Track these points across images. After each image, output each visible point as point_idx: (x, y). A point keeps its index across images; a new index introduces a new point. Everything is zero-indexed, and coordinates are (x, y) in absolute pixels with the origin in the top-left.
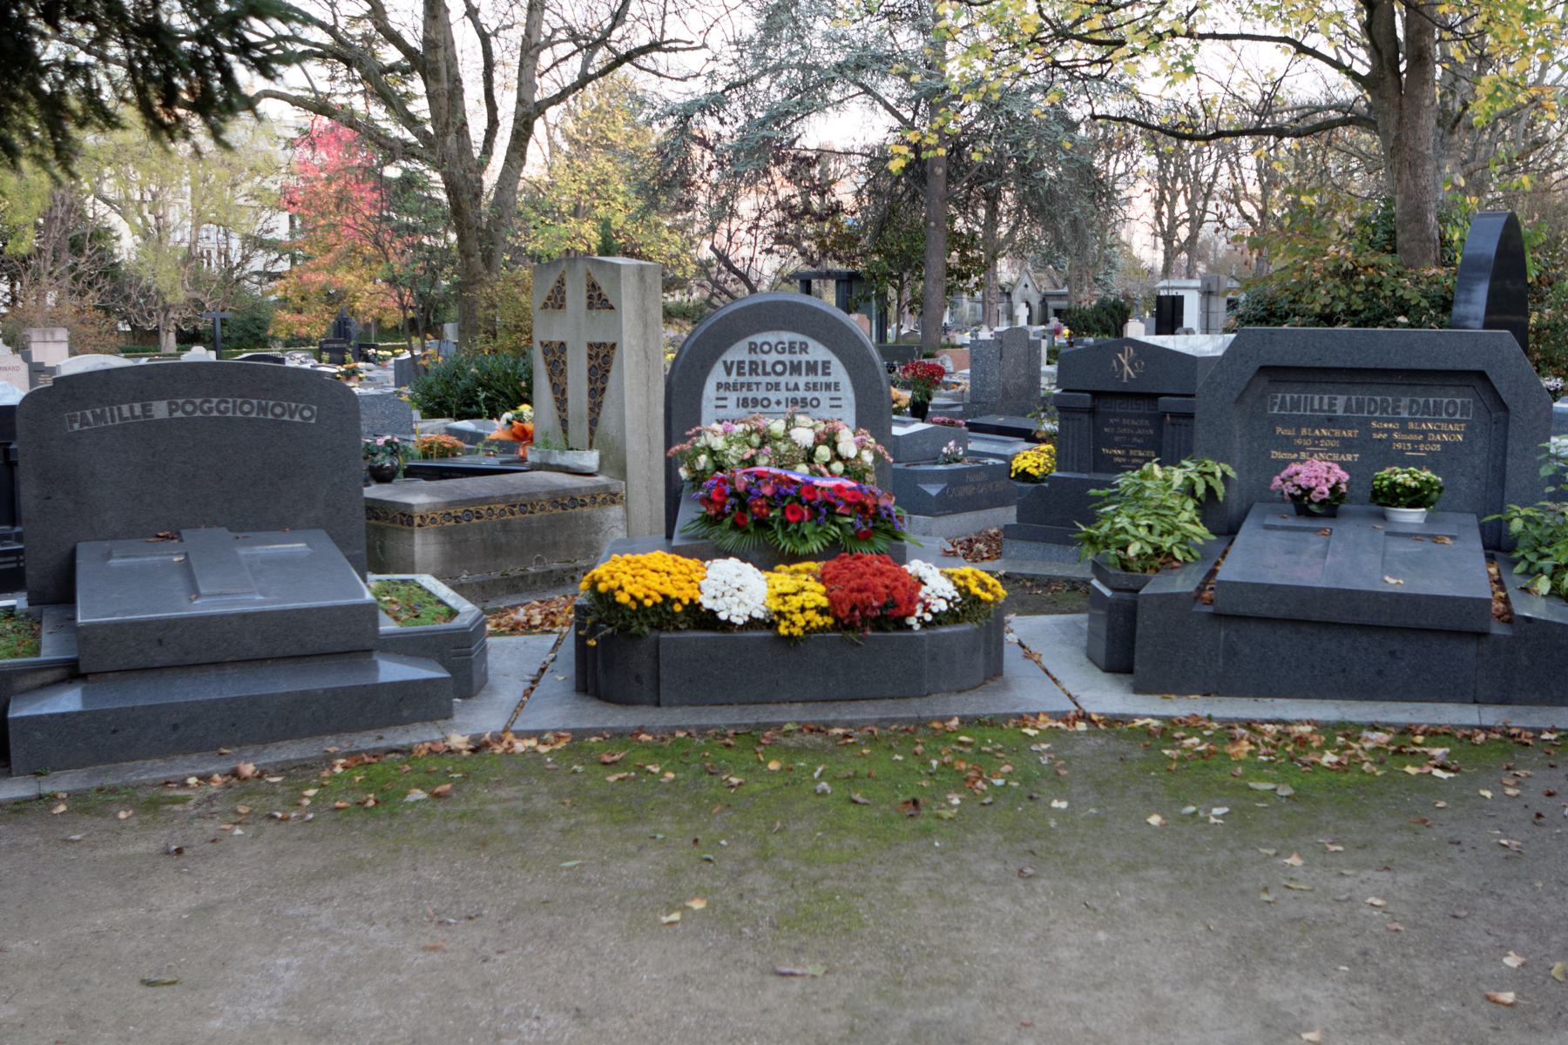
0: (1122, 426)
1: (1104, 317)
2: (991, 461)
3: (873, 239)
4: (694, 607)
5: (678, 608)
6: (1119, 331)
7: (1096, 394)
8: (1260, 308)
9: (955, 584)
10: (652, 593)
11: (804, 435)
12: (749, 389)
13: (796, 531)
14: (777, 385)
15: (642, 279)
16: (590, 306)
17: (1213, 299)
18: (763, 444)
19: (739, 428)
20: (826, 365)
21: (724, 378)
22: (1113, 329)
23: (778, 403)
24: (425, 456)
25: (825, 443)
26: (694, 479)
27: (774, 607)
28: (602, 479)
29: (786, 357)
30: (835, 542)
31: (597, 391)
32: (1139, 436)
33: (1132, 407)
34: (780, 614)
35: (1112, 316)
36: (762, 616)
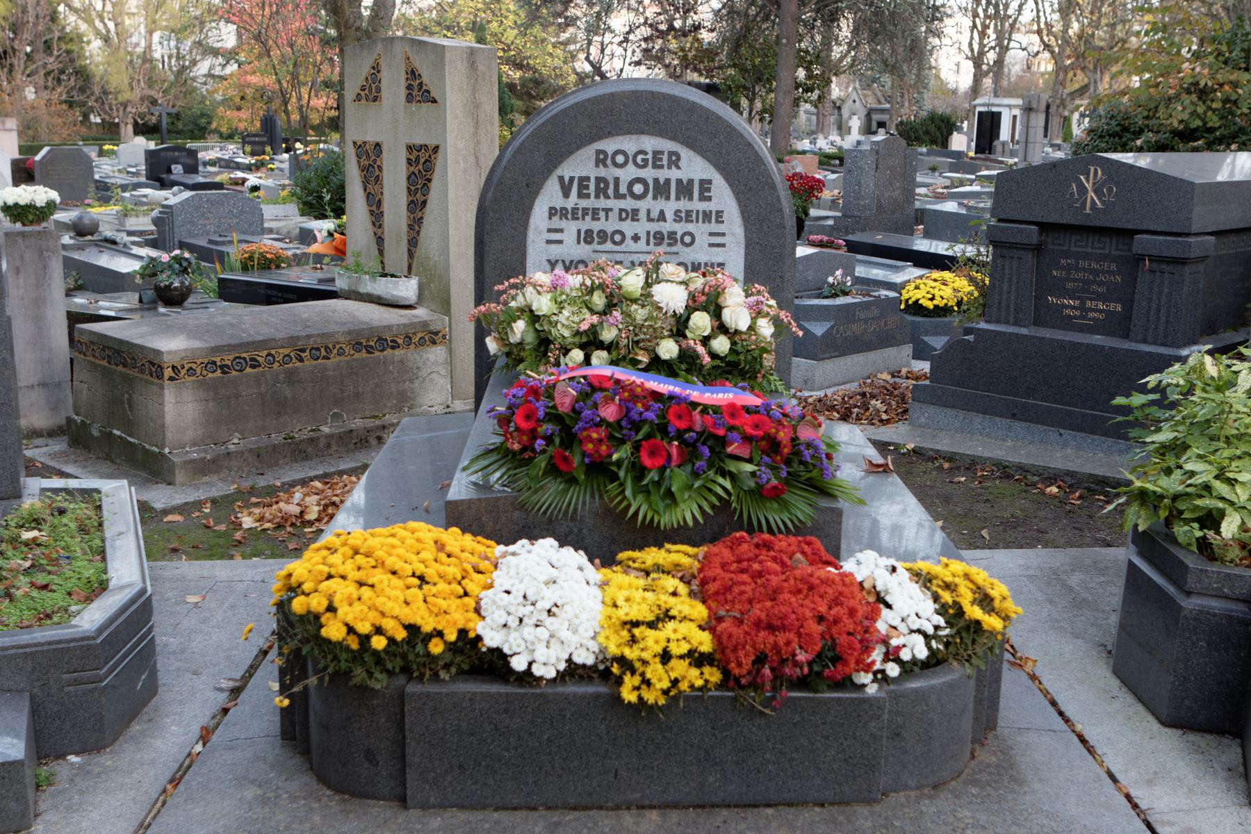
0: (1077, 269)
1: (933, 129)
2: (884, 293)
3: (729, 55)
4: (467, 642)
5: (436, 647)
6: (945, 143)
7: (1044, 227)
8: (1114, 123)
9: (936, 598)
10: (389, 625)
11: (671, 296)
12: (595, 218)
13: (658, 484)
14: (635, 212)
15: (473, 65)
16: (410, 98)
17: (1033, 115)
18: (610, 306)
19: (574, 281)
20: (705, 185)
21: (559, 202)
22: (940, 140)
23: (636, 238)
24: (245, 268)
25: (705, 309)
26: (508, 354)
27: (613, 650)
28: (421, 313)
29: (648, 173)
30: (724, 506)
31: (417, 206)
32: (1100, 284)
33: (1093, 246)
34: (622, 660)
35: (939, 128)
36: (590, 661)
